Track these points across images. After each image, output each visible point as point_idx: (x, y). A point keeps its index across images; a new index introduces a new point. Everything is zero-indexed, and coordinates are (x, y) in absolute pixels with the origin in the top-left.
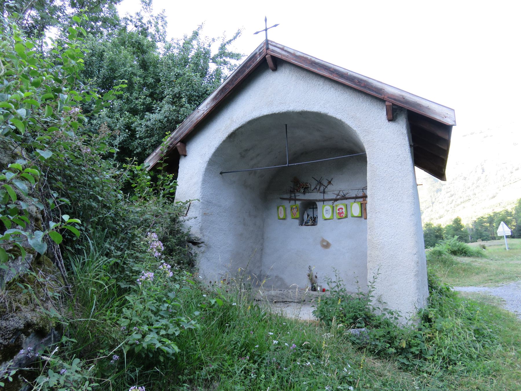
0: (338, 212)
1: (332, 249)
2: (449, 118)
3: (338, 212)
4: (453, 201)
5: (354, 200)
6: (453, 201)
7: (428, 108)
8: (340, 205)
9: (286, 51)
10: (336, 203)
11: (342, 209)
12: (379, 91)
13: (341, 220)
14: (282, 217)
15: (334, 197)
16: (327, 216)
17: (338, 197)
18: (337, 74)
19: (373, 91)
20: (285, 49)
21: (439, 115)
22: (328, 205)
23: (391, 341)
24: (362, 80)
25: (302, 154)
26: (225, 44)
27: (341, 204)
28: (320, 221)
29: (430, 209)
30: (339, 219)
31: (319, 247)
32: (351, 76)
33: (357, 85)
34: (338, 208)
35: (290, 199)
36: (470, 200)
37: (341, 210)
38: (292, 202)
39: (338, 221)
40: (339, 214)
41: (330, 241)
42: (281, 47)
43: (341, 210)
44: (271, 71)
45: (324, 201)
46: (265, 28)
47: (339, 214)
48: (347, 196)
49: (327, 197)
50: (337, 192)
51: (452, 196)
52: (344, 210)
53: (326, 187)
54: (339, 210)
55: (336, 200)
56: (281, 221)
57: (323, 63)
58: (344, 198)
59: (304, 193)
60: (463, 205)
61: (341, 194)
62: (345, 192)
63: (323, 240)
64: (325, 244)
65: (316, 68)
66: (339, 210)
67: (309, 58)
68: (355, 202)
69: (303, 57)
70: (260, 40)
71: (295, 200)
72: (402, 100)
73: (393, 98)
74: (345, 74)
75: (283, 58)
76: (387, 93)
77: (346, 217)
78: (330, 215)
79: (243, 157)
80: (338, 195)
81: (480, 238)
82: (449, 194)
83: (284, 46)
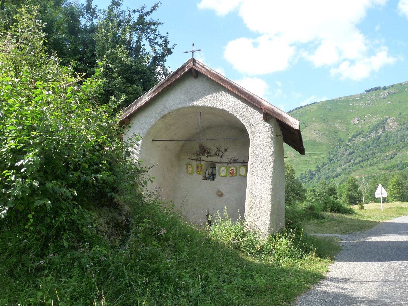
0: (230, 172)
1: (223, 198)
2: (296, 125)
3: (230, 172)
4: (351, 159)
5: (242, 164)
6: (351, 159)
7: (285, 118)
8: (232, 167)
9: (205, 68)
10: (229, 165)
11: (233, 170)
12: (260, 103)
13: (232, 178)
14: (190, 172)
15: (228, 161)
16: (223, 174)
17: (232, 161)
18: (236, 89)
19: (256, 103)
20: (205, 66)
21: (291, 123)
22: (224, 166)
23: (253, 246)
24: (250, 95)
25: (208, 128)
26: (144, 16)
27: (233, 166)
28: (217, 177)
29: (327, 167)
30: (231, 177)
31: (216, 196)
32: (244, 91)
33: (247, 98)
34: (231, 169)
35: (196, 160)
36: (368, 159)
37: (232, 170)
38: (198, 162)
39: (230, 178)
40: (231, 173)
41: (223, 192)
42: (202, 65)
43: (232, 170)
44: (193, 78)
45: (220, 163)
46: (192, 50)
47: (231, 173)
48: (237, 161)
49: (223, 160)
50: (230, 158)
51: (351, 154)
52: (234, 171)
53: (223, 153)
54: (231, 170)
55: (229, 163)
56: (189, 175)
57: (228, 80)
58: (235, 162)
59: (207, 156)
60: (361, 164)
61: (233, 159)
62: (236, 158)
63: (219, 191)
64: (220, 193)
65: (223, 83)
66: (231, 170)
67: (220, 75)
68: (242, 166)
69: (216, 74)
70: (188, 57)
71: (200, 161)
72: (272, 111)
73: (267, 108)
74: (241, 90)
75: (203, 72)
76: (264, 106)
77: (236, 175)
78: (225, 174)
79: (168, 129)
80: (231, 159)
81: (373, 200)
82: (347, 152)
83: (204, 65)
